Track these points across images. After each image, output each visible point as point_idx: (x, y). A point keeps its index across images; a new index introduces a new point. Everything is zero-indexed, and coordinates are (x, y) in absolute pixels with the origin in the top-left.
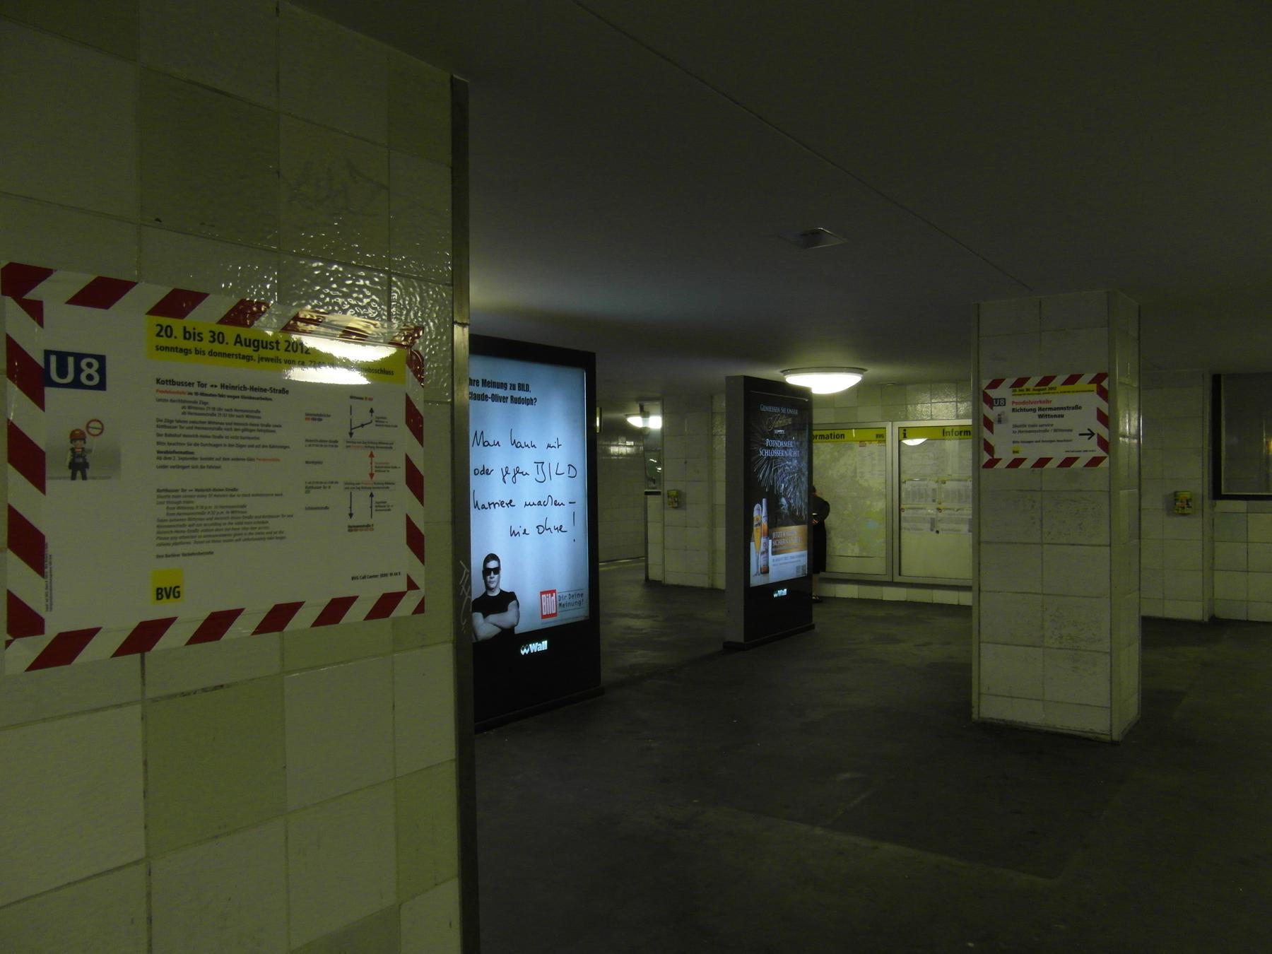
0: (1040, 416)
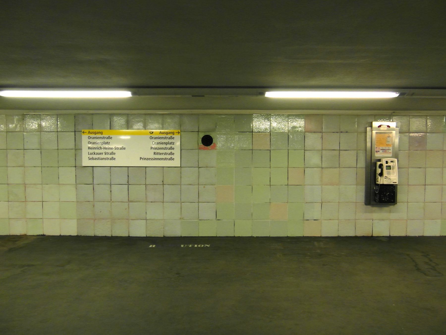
0: (155, 153)
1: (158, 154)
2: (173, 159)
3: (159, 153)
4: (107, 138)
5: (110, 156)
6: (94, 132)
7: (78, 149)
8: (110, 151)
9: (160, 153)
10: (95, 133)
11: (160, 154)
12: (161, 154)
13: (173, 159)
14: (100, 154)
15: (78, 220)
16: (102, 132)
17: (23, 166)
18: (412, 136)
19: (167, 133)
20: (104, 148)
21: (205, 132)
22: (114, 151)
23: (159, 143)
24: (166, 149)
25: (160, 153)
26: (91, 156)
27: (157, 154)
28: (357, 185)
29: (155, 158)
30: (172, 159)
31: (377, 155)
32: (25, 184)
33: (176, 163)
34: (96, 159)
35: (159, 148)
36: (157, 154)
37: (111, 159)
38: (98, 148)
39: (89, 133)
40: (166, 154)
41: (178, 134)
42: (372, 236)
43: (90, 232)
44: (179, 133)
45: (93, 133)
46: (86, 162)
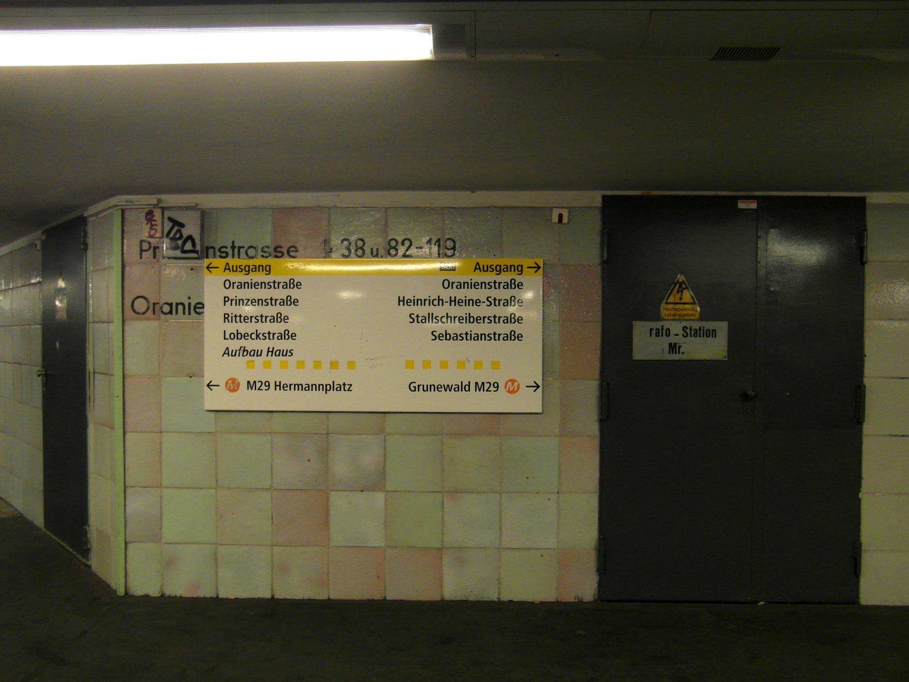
1: (238, 319)
2: (519, 337)
3: (240, 316)
5: (503, 329)
6: (243, 267)
9: (243, 315)
10: (248, 270)
11: (244, 319)
13: (519, 337)
16: (270, 266)
19: (498, 268)
20: (451, 301)
23: (245, 283)
24: (273, 303)
25: (243, 315)
27: (234, 318)
29: (469, 300)
30: (516, 335)
34: (456, 337)
35: (249, 300)
36: (234, 318)
37: (507, 338)
39: (225, 269)
41: (536, 272)
44: (539, 267)
45: (239, 269)
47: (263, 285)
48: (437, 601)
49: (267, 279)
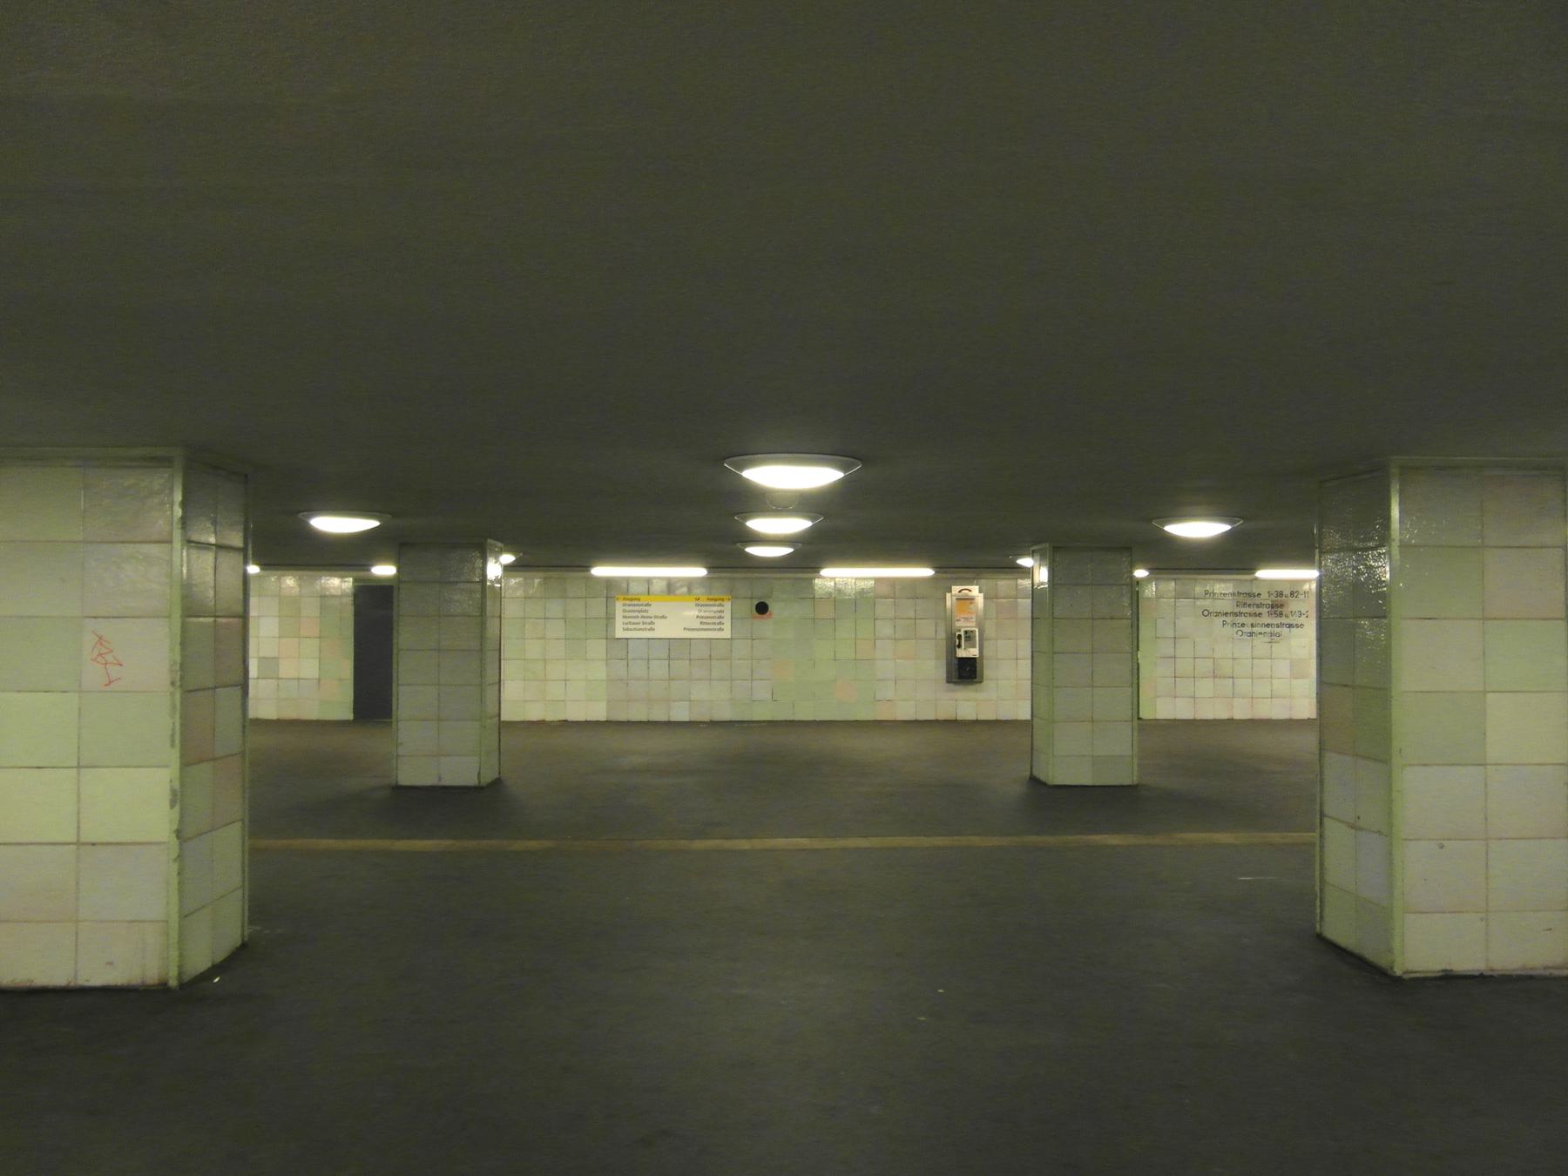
0: (701, 623)
4: (646, 605)
7: (610, 618)
8: (649, 620)
10: (631, 600)
12: (709, 624)
14: (636, 624)
15: (609, 701)
17: (543, 638)
18: (249, 907)
21: (760, 598)
22: (653, 620)
26: (626, 627)
28: (936, 659)
31: (958, 624)
32: (545, 660)
33: (727, 634)
34: (631, 630)
38: (635, 617)
40: (714, 623)
42: (956, 720)
43: (622, 717)
46: (620, 633)
47: (637, 605)
48: (209, 969)
49: (639, 603)
